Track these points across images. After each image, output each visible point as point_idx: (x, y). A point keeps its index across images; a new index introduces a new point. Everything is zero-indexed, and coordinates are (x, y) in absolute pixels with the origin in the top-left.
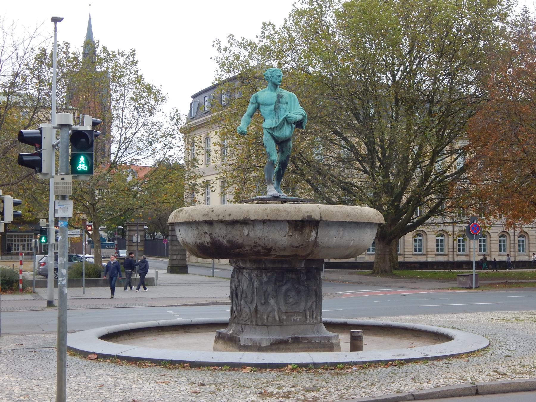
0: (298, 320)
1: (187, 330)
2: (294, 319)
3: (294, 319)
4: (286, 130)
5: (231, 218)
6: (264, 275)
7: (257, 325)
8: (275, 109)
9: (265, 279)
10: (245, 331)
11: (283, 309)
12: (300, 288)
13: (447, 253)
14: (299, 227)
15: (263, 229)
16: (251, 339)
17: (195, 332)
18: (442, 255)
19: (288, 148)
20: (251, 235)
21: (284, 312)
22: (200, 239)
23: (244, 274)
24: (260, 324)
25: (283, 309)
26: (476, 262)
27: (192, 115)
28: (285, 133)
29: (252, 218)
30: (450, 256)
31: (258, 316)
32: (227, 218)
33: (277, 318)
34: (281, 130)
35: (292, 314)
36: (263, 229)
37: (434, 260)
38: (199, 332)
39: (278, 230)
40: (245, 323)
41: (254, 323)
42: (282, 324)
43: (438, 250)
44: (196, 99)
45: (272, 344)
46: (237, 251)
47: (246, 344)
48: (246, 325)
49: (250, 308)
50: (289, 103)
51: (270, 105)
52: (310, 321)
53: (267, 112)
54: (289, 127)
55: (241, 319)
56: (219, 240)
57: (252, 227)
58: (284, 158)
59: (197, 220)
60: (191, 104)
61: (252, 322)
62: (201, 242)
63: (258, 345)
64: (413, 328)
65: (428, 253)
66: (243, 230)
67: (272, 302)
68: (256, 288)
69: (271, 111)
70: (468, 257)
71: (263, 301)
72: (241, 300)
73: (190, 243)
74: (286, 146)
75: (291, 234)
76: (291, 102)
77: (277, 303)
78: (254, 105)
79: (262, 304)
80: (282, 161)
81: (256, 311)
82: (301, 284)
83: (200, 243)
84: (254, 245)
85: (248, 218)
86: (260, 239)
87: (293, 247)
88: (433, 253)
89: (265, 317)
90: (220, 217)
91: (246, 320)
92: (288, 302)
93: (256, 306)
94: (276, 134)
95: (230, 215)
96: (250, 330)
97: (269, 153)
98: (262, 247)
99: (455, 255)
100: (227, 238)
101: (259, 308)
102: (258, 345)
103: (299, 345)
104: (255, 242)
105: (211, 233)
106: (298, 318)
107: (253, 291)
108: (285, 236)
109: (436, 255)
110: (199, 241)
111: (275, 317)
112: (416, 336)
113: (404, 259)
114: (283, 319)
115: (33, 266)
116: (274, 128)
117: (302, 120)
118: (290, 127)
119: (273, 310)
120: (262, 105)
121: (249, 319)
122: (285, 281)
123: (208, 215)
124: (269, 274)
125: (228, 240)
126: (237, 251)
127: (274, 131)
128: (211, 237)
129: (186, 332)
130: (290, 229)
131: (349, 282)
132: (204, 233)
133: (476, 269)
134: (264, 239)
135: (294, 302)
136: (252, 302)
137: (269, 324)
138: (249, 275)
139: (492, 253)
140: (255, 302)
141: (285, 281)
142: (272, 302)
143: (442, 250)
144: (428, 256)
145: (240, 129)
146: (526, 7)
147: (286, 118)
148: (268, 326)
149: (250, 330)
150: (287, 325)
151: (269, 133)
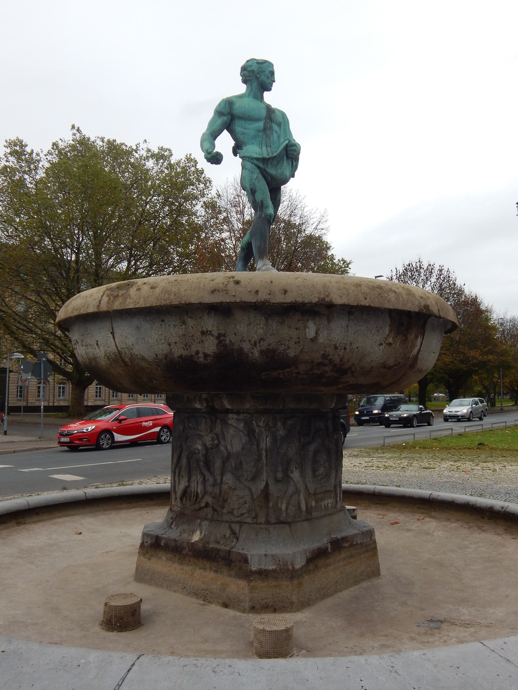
1: (21, 520)
5: (289, 299)
6: (279, 424)
7: (268, 522)
8: (265, 129)
9: (282, 432)
10: (242, 537)
11: (311, 487)
13: (103, 398)
14: (403, 328)
15: (347, 326)
16: (273, 556)
17: (34, 522)
18: (99, 400)
20: (321, 339)
22: (187, 346)
23: (230, 422)
24: (273, 520)
25: (311, 487)
26: (24, 407)
29: (338, 300)
30: (106, 401)
31: (271, 505)
32: (279, 299)
33: (303, 507)
36: (347, 326)
37: (93, 404)
38: (40, 521)
39: (373, 332)
40: (238, 519)
41: (262, 520)
42: (309, 517)
43: (96, 396)
45: (309, 561)
46: (275, 374)
47: (263, 567)
48: (241, 523)
49: (250, 489)
50: (282, 125)
51: (258, 120)
53: (253, 133)
55: (225, 511)
56: (241, 349)
57: (326, 323)
59: (194, 300)
61: (256, 517)
62: (185, 353)
63: (290, 567)
64: (374, 492)
65: (89, 398)
66: (306, 327)
67: (296, 475)
68: (266, 451)
69: (259, 131)
70: (120, 402)
71: (280, 475)
72: (222, 475)
73: (143, 359)
75: (390, 340)
78: (225, 118)
79: (277, 481)
81: (266, 494)
83: (181, 357)
84: (321, 360)
85: (327, 299)
86: (336, 348)
87: (385, 367)
88: (93, 398)
89: (284, 507)
90: (260, 295)
91: (242, 514)
92: (317, 473)
93: (267, 485)
95: (285, 292)
96: (257, 535)
97: (262, 202)
98: (335, 365)
99: (110, 400)
100: (264, 345)
101: (273, 489)
102: (290, 567)
103: (340, 555)
104: (324, 355)
105: (222, 332)
107: (260, 455)
108: (381, 344)
109: (95, 400)
110: (178, 351)
111: (299, 504)
112: (378, 504)
113: (88, 404)
114: (311, 506)
115: (204, 395)
116: (268, 159)
121: (249, 511)
123: (227, 292)
124: (290, 422)
125: (263, 348)
126: (275, 374)
127: (267, 166)
128: (220, 342)
129: (19, 524)
130: (390, 331)
131: (50, 425)
132: (203, 333)
133: (23, 412)
134: (345, 349)
136: (254, 478)
137: (290, 520)
138: (246, 424)
139: (123, 398)
140: (264, 476)
143: (100, 396)
144: (89, 401)
146: (218, 192)
147: (287, 146)
148: (289, 523)
149: (257, 535)
150: (316, 518)
151: (259, 167)
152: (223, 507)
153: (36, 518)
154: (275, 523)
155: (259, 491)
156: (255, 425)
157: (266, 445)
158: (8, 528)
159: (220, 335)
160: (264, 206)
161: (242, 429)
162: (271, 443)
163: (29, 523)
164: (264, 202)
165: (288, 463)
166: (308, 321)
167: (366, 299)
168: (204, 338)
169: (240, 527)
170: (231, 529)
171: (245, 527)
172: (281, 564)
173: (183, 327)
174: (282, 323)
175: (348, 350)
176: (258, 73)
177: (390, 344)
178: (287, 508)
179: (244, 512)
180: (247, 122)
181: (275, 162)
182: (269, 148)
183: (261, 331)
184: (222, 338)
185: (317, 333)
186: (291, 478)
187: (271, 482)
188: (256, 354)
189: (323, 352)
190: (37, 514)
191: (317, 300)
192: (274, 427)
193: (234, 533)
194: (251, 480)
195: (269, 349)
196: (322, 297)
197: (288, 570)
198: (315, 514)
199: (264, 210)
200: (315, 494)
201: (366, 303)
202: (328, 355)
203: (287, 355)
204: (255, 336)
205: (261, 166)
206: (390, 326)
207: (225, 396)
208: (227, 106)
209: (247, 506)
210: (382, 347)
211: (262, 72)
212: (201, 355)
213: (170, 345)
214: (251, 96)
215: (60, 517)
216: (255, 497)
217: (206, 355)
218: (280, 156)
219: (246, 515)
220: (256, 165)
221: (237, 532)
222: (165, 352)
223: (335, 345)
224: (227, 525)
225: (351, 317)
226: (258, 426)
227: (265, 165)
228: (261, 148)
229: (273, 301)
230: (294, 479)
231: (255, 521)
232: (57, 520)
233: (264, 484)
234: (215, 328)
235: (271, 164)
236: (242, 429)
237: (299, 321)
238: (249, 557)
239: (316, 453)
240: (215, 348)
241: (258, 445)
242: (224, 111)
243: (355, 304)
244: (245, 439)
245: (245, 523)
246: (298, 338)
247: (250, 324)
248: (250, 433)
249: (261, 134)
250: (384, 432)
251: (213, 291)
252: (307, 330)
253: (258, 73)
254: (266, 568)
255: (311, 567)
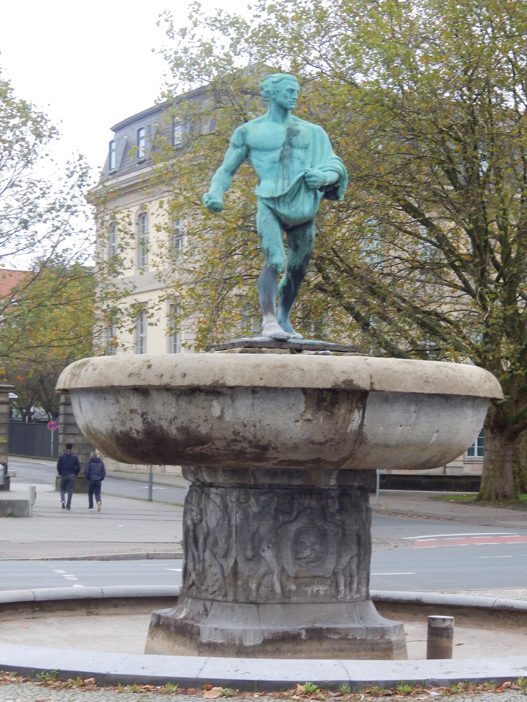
0: (322, 592)
2: (312, 591)
3: (312, 591)
4: (303, 202)
5: (186, 382)
6: (253, 500)
7: (236, 601)
8: (281, 159)
9: (255, 509)
10: (211, 613)
12: (326, 527)
14: (325, 404)
15: (253, 405)
16: (222, 630)
17: (110, 615)
19: (308, 239)
20: (228, 417)
21: (292, 575)
22: (123, 423)
23: (212, 496)
24: (242, 598)
25: (291, 569)
27: (113, 166)
28: (301, 209)
31: (240, 583)
32: (179, 382)
33: (278, 589)
34: (294, 203)
35: (309, 580)
36: (253, 405)
38: (117, 614)
41: (230, 598)
42: (287, 600)
44: (121, 133)
45: (265, 642)
47: (213, 640)
48: (213, 600)
49: (222, 567)
50: (311, 147)
52: (345, 596)
54: (310, 197)
56: (161, 427)
57: (230, 402)
58: (299, 261)
59: (116, 384)
60: (111, 143)
61: (225, 595)
62: (123, 429)
66: (211, 406)
67: (268, 554)
68: (236, 527)
69: (274, 162)
71: (249, 554)
72: (204, 551)
73: (101, 433)
74: (304, 235)
75: (309, 416)
76: (315, 145)
77: (278, 556)
78: (239, 151)
80: (295, 267)
81: (235, 573)
82: (329, 520)
83: (121, 432)
84: (233, 437)
85: (221, 382)
86: (245, 426)
87: (313, 443)
91: (215, 592)
92: (301, 555)
94: (283, 210)
95: (185, 375)
96: (222, 612)
97: (268, 249)
98: (250, 442)
100: (178, 423)
101: (242, 567)
103: (321, 645)
104: (234, 432)
105: (144, 411)
106: (321, 588)
108: (297, 421)
110: (119, 428)
111: (272, 586)
114: (290, 590)
116: (279, 198)
117: (337, 182)
118: (312, 196)
119: (269, 572)
120: (256, 149)
121: (220, 588)
122: (295, 514)
124: (263, 498)
125: (179, 426)
127: (279, 205)
128: (144, 420)
129: (90, 614)
130: (307, 408)
134: (255, 426)
135: (313, 555)
136: (226, 555)
140: (233, 554)
141: (295, 514)
142: (268, 554)
145: (210, 199)
147: (303, 177)
149: (222, 612)
151: (269, 208)
152: (202, 585)
153: (113, 610)
154: (244, 603)
155: (230, 568)
156: (229, 500)
157: (236, 521)
158: (75, 616)
159: (143, 414)
160: (270, 254)
161: (219, 504)
162: (241, 519)
163: (102, 615)
164: (270, 249)
165: (261, 541)
166: (212, 401)
167: (262, 379)
168: (133, 416)
169: (212, 604)
170: (205, 606)
171: (215, 604)
172: (229, 638)
173: (118, 405)
174: (190, 403)
175: (258, 427)
176: (274, 94)
177: (309, 420)
178: (258, 588)
179: (216, 589)
180: (263, 153)
181: (288, 200)
182: (286, 181)
183: (173, 410)
184: (145, 416)
185: (222, 412)
186: (263, 558)
187: (241, 560)
188: (174, 431)
189: (232, 430)
190: (116, 606)
191: (211, 382)
192: (246, 502)
193: (206, 610)
194: (223, 557)
195: (182, 427)
196: (216, 379)
197: (235, 645)
198: (294, 599)
199: (270, 259)
200: (296, 578)
201: (261, 384)
202: (239, 433)
203: (200, 432)
204: (170, 415)
205: (272, 206)
206: (306, 402)
207: (204, 468)
208: (240, 137)
209: (218, 583)
210: (298, 424)
211: (278, 92)
212: (134, 431)
213: (112, 421)
214: (271, 119)
215: (145, 614)
216: (226, 575)
217: (138, 432)
218: (294, 191)
219: (217, 593)
220: (266, 206)
221: (209, 609)
222: (111, 427)
223: (243, 422)
224: (202, 602)
225: (255, 396)
226: (231, 501)
227: (277, 204)
228: (276, 182)
229: (173, 384)
230: (267, 559)
231: (225, 599)
232: (139, 616)
233: (233, 561)
234: (139, 407)
235: (283, 202)
236: (219, 504)
237: (204, 401)
238: (201, 629)
239: (299, 533)
240: (142, 425)
241: (230, 521)
242: (237, 143)
243: (249, 385)
244: (219, 514)
245: (217, 601)
246: (206, 416)
247: (164, 404)
248: (225, 508)
249: (277, 165)
250: (395, 513)
251: (130, 375)
252: (212, 409)
253: (274, 94)
254: (215, 641)
255: (269, 648)
